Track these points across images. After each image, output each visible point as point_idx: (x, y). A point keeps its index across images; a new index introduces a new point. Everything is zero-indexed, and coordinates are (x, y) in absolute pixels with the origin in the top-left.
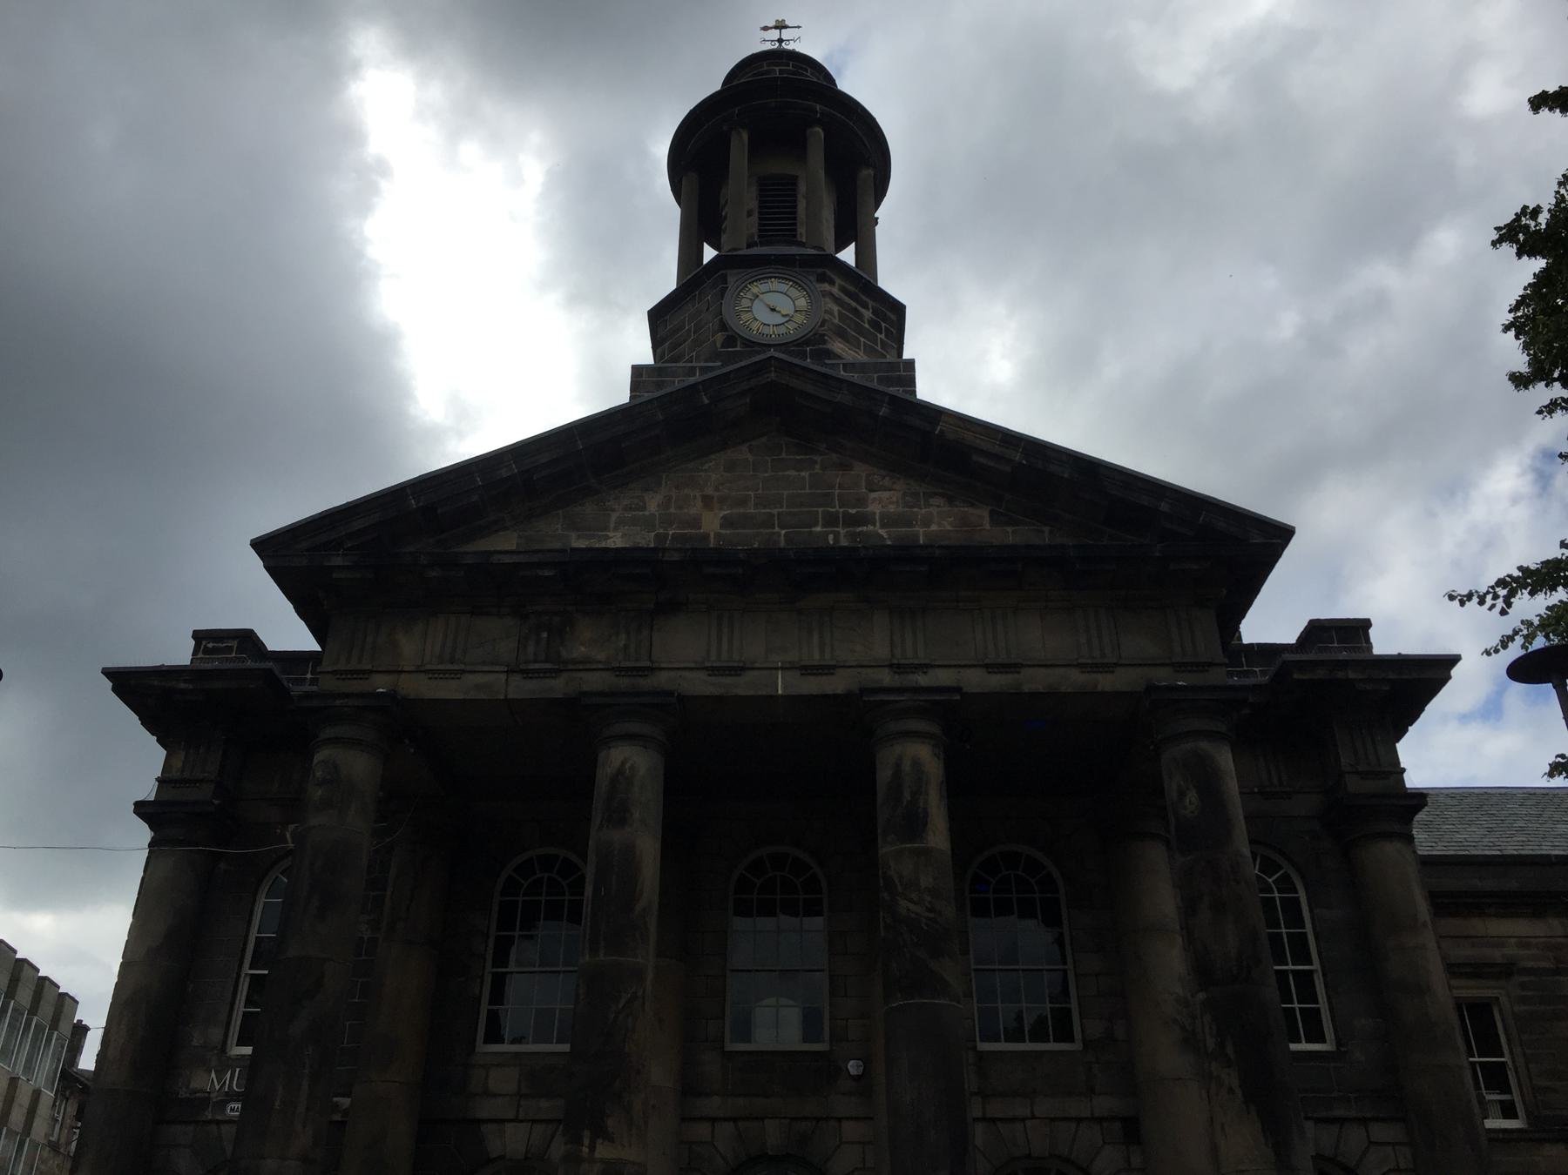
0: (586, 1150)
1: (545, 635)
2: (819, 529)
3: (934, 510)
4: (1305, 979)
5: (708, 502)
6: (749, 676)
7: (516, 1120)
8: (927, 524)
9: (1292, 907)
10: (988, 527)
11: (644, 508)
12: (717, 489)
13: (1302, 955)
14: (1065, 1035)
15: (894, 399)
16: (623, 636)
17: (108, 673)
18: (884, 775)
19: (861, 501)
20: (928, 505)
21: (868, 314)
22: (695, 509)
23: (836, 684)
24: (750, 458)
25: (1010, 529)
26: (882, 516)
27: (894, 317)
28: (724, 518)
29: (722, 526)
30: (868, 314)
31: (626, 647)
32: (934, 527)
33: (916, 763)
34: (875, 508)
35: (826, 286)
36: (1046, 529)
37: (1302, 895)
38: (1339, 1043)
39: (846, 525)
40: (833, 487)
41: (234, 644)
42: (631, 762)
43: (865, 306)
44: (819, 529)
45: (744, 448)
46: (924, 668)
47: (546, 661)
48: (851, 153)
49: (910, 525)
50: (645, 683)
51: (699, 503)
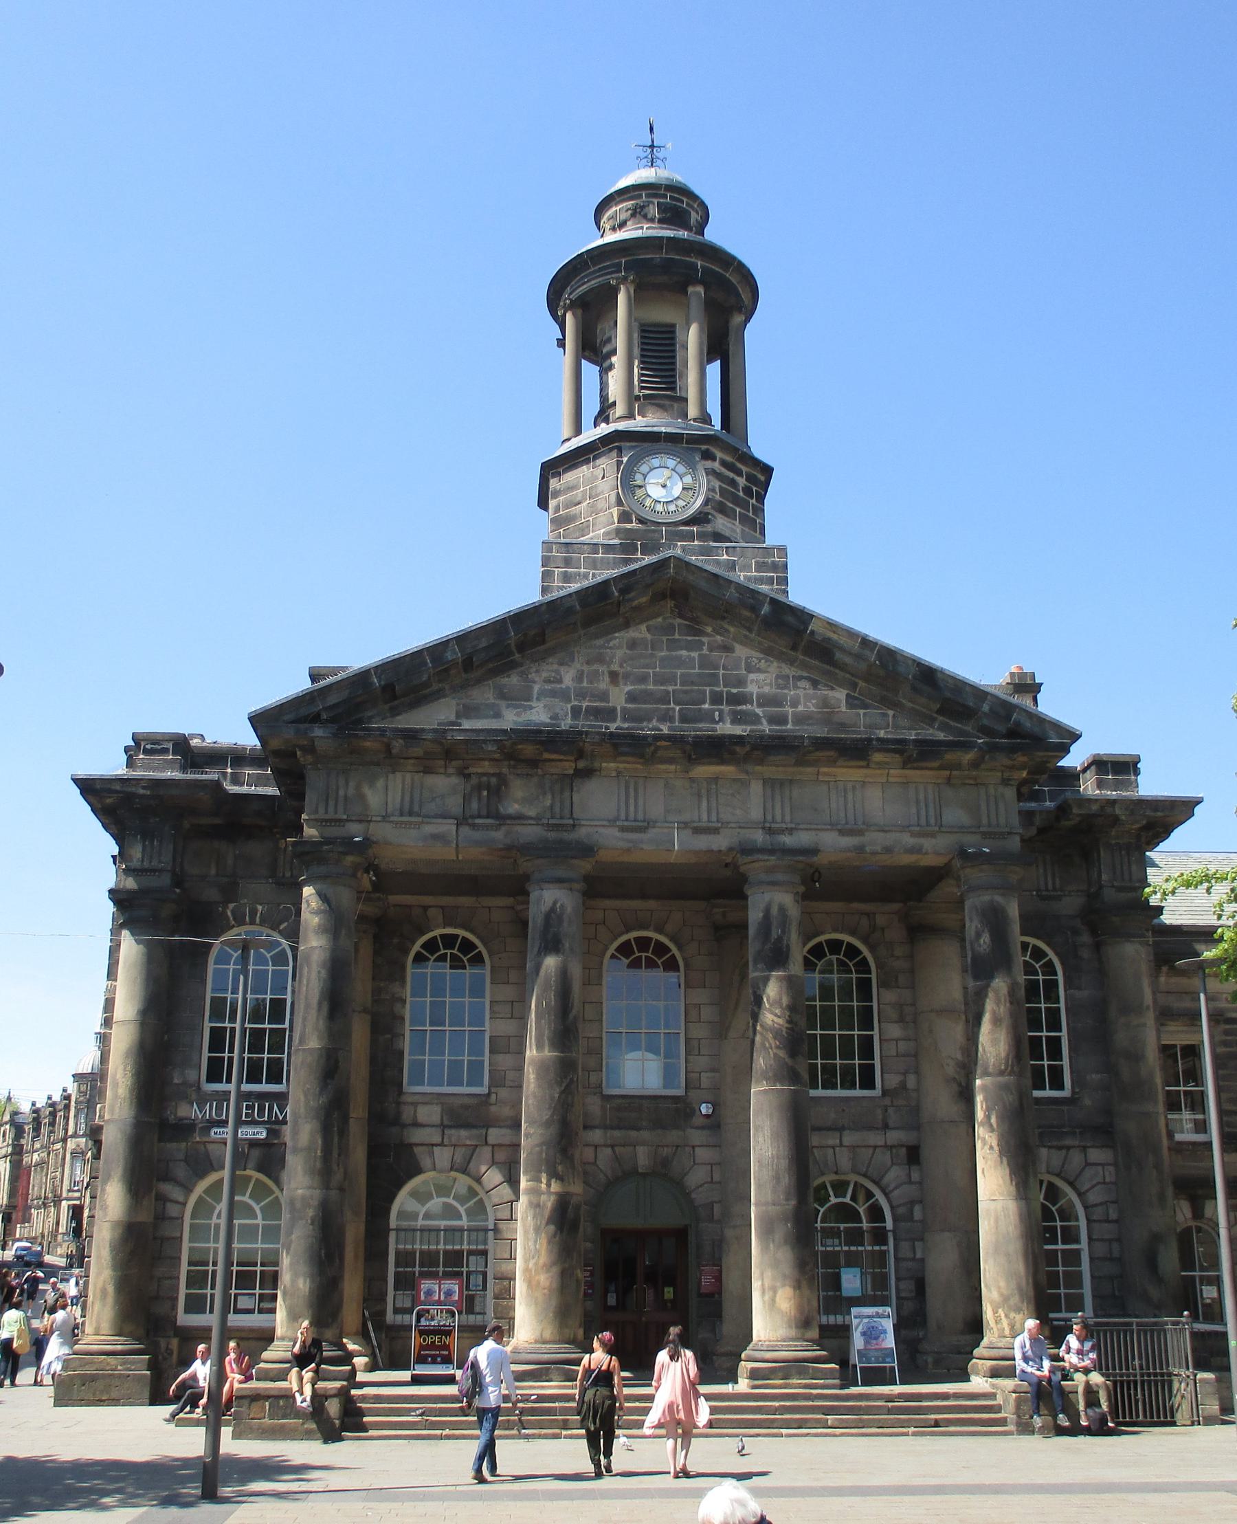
0: (544, 1186)
1: (485, 793)
2: (707, 706)
3: (801, 692)
4: (1055, 1044)
5: (614, 676)
6: (652, 833)
7: (442, 1144)
8: (795, 704)
9: (1051, 986)
10: (844, 709)
11: (560, 681)
12: (621, 666)
13: (1055, 1025)
14: (868, 1083)
15: (774, 601)
16: (550, 797)
17: (78, 781)
18: (754, 916)
19: (741, 682)
20: (796, 687)
21: (742, 481)
22: (604, 684)
23: (720, 842)
24: (649, 636)
25: (862, 712)
26: (759, 696)
27: (762, 478)
28: (628, 693)
29: (627, 702)
30: (742, 481)
31: (552, 806)
32: (801, 708)
33: (782, 909)
34: (752, 689)
35: (709, 464)
36: (891, 713)
37: (1060, 978)
38: (1073, 1092)
39: (728, 703)
40: (717, 668)
41: (170, 746)
42: (771, 900)
43: (739, 473)
44: (707, 706)
45: (643, 627)
46: (791, 831)
47: (488, 817)
48: (726, 293)
49: (781, 705)
50: (566, 836)
51: (607, 679)
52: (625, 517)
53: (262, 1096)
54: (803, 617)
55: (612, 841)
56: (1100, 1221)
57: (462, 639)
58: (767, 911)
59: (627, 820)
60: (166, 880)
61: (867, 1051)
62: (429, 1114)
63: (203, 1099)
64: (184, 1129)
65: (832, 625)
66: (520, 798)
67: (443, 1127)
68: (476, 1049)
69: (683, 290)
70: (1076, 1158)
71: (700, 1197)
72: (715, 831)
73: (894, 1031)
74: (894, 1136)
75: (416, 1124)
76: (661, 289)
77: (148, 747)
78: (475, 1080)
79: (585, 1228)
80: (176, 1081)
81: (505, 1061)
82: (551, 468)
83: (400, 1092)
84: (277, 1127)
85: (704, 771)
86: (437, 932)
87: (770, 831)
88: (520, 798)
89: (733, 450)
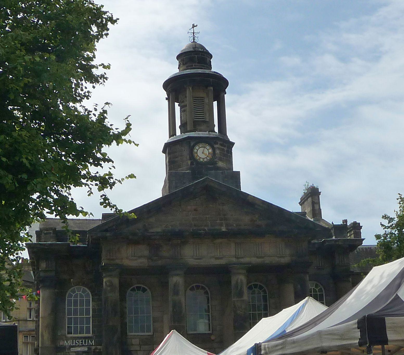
18: (233, 283)
23: (222, 262)
33: (241, 280)
42: (240, 278)
48: (218, 86)
53: (85, 338)
55: (192, 262)
56: (203, 151)
58: (237, 282)
59: (196, 256)
60: (53, 274)
62: (136, 341)
63: (67, 339)
66: (166, 252)
67: (140, 345)
69: (207, 87)
72: (221, 258)
75: (132, 345)
77: (45, 232)
78: (149, 331)
80: (59, 334)
83: (126, 335)
84: (90, 347)
85: (219, 241)
86: (135, 286)
87: (237, 258)
88: (166, 252)
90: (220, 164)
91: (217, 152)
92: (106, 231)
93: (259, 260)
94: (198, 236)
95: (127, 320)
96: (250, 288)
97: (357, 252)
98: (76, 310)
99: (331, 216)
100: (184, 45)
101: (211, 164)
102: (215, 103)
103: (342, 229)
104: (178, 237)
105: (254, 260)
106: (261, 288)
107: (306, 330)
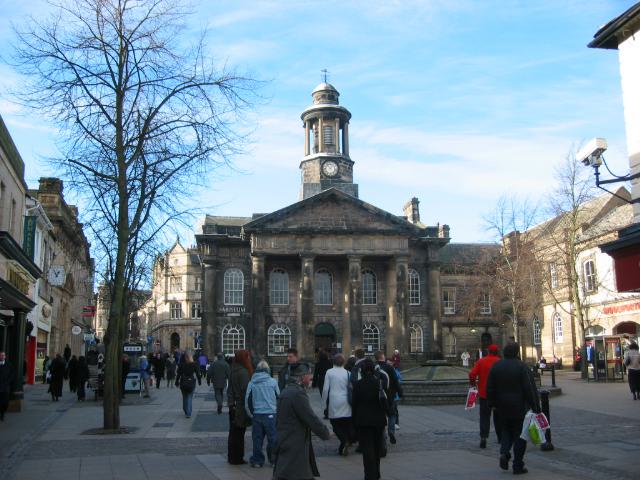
14: (417, 301)
18: (351, 267)
42: (355, 265)
52: (321, 177)
54: (362, 202)
57: (287, 208)
61: (375, 295)
64: (222, 314)
65: (368, 204)
68: (286, 295)
70: (421, 319)
71: (336, 328)
73: (380, 290)
74: (380, 314)
76: (332, 116)
79: (250, 366)
81: (293, 298)
82: (302, 163)
89: (345, 159)
90: (343, 178)
91: (341, 168)
92: (255, 226)
93: (371, 252)
94: (325, 233)
95: (270, 295)
96: (363, 273)
97: (207, 263)
98: (231, 285)
99: (426, 221)
100: (563, 391)
101: (336, 177)
102: (341, 131)
103: (433, 231)
104: (308, 233)
105: (368, 252)
106: (371, 273)
107: (602, 34)
